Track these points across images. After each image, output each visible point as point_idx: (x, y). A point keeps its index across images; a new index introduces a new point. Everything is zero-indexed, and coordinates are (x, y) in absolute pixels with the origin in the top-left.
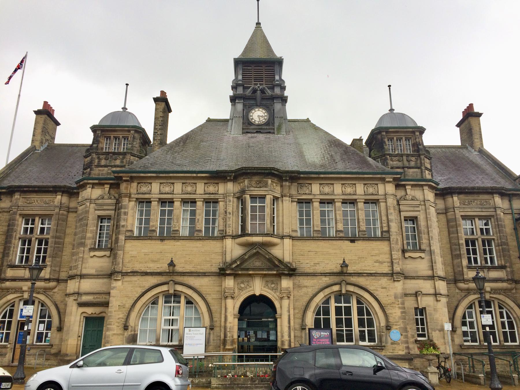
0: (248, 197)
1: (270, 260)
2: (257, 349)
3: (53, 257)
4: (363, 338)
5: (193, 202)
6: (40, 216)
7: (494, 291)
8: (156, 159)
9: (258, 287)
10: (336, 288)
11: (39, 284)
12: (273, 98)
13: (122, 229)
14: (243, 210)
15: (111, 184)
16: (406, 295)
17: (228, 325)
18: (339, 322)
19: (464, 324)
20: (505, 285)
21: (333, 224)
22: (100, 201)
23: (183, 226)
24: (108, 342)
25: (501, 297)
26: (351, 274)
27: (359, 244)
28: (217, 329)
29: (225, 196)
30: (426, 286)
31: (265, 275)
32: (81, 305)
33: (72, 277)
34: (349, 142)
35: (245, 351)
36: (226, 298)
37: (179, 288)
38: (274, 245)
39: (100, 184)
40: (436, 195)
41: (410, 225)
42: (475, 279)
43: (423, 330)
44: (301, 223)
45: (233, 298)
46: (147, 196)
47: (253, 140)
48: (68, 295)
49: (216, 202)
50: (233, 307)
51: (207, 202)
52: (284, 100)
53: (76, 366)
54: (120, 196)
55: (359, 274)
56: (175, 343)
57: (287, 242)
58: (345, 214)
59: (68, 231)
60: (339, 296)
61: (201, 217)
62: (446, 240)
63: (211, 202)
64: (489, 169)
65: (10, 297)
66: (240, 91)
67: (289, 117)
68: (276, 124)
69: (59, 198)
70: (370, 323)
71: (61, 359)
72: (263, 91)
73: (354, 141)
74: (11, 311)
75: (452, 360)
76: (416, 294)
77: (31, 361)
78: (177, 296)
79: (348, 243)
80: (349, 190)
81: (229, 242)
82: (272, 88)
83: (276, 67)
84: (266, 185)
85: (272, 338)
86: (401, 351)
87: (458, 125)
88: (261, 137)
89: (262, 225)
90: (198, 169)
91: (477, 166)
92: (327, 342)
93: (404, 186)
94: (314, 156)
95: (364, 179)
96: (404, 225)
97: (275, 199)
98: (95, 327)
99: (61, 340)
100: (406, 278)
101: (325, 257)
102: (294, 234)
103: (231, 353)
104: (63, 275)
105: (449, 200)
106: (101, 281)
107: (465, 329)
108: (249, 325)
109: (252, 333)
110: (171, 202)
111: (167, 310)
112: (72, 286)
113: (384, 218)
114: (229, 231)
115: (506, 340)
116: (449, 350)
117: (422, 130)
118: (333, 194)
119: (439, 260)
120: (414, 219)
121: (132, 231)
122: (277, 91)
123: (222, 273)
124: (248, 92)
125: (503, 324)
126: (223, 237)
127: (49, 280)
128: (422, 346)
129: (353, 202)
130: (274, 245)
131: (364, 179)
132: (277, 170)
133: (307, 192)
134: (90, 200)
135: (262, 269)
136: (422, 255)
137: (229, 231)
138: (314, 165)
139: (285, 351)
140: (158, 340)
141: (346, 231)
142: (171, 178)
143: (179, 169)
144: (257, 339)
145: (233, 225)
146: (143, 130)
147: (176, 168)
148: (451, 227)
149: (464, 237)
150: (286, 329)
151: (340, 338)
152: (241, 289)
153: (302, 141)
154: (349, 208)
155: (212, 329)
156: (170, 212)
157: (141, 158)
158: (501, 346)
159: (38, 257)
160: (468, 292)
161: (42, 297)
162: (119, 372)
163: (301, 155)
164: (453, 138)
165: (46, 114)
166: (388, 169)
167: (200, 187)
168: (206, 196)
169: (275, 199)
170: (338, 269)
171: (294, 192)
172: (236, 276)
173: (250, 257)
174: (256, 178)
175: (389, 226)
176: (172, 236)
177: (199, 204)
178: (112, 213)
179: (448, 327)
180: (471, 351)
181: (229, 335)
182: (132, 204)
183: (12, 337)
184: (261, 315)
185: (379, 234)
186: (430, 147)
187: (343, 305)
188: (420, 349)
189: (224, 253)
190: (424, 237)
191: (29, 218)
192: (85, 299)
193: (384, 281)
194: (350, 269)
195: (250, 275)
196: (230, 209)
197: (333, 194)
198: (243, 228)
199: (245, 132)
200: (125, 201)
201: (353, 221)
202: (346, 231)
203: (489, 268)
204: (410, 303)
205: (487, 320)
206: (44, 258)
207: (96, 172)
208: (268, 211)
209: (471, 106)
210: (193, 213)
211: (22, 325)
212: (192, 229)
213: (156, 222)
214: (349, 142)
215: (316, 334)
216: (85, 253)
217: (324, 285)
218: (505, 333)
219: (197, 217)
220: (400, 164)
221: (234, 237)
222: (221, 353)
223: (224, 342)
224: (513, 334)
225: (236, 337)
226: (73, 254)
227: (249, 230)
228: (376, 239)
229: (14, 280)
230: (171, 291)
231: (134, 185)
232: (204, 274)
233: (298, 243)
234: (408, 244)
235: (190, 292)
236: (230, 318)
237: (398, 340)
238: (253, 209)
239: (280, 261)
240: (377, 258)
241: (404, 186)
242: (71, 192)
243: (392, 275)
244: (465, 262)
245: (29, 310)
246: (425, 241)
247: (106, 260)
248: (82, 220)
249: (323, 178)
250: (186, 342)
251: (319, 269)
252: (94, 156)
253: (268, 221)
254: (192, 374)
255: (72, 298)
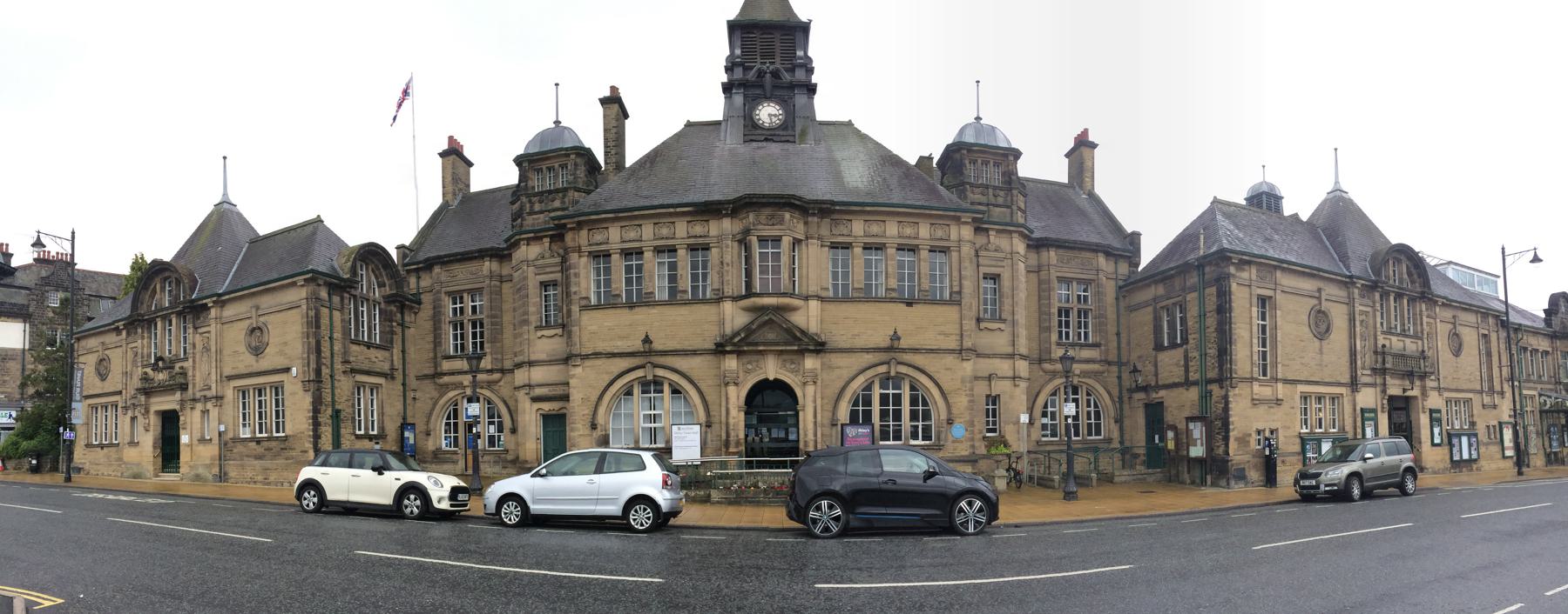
0: (754, 239)
1: (789, 331)
2: (772, 453)
3: (493, 341)
4: (915, 436)
5: (672, 250)
6: (469, 291)
7: (1084, 374)
8: (611, 193)
9: (771, 369)
10: (883, 369)
11: (481, 377)
12: (792, 86)
13: (574, 297)
14: (748, 259)
15: (552, 237)
16: (977, 378)
17: (731, 421)
18: (884, 415)
19: (1044, 415)
20: (1096, 367)
21: (882, 279)
22: (541, 262)
23: (658, 285)
24: (573, 446)
25: (1090, 381)
26: (904, 350)
27: (916, 308)
28: (715, 427)
29: (720, 238)
30: (1004, 367)
31: (781, 353)
32: (535, 399)
33: (519, 366)
34: (913, 161)
35: (755, 453)
36: (727, 384)
37: (660, 372)
38: (794, 309)
39: (538, 239)
40: (1028, 246)
41: (990, 285)
42: (1063, 359)
43: (994, 423)
44: (835, 277)
45: (736, 384)
46: (603, 247)
47: (761, 152)
48: (517, 388)
49: (706, 248)
50: (736, 396)
51: (693, 249)
52: (811, 89)
53: (537, 475)
54: (566, 250)
55: (916, 351)
56: (660, 445)
57: (814, 305)
58: (901, 265)
59: (506, 306)
60: (885, 380)
61: (685, 272)
62: (1035, 306)
63: (698, 248)
64: (1097, 219)
65: (452, 394)
66: (738, 73)
67: (820, 117)
68: (798, 129)
69: (488, 266)
70: (927, 415)
71: (520, 466)
72: (776, 74)
73: (921, 158)
74: (456, 411)
75: (1026, 459)
76: (990, 378)
77: (486, 469)
78: (657, 384)
79: (903, 306)
80: (908, 231)
81: (728, 306)
82: (792, 70)
83: (799, 36)
84: (781, 222)
85: (792, 437)
86: (963, 450)
87: (1067, 156)
88: (774, 148)
89: (777, 281)
90: (676, 201)
91: (1082, 213)
92: (867, 442)
93: (987, 230)
94: (856, 176)
95: (931, 216)
96: (983, 284)
97: (796, 242)
98: (555, 426)
99: (517, 444)
100: (979, 355)
101: (865, 326)
102: (824, 294)
103: (736, 458)
104: (508, 364)
105: (1044, 254)
106: (555, 368)
107: (1045, 421)
108: (761, 420)
109: (764, 430)
110: (640, 253)
111: (647, 404)
112: (521, 376)
113: (955, 274)
114: (728, 291)
115: (1090, 434)
116: (1023, 447)
117: (1017, 154)
118: (884, 236)
119: (1022, 333)
120: (995, 278)
121: (587, 298)
122: (800, 75)
123: (720, 350)
124: (751, 75)
125: (1089, 413)
126: (719, 299)
127: (491, 371)
128: (991, 443)
129: (913, 249)
130: (794, 309)
131: (931, 216)
132: (800, 199)
133: (845, 232)
134: (527, 262)
135: (777, 344)
136: (1002, 326)
137: (728, 291)
138: (856, 191)
139: (808, 454)
140: (637, 442)
141: (901, 289)
142: (636, 217)
143: (647, 203)
144: (772, 440)
145: (735, 284)
146: (589, 151)
147: (642, 203)
148: (1043, 291)
149: (1057, 305)
150: (810, 426)
151: (885, 436)
152: (747, 372)
153: (838, 155)
154: (907, 258)
155: (709, 425)
156: (640, 268)
157: (589, 192)
158: (1084, 442)
159: (475, 344)
160: (1054, 374)
161: (487, 393)
162: (591, 482)
163: (838, 176)
164: (1056, 171)
165: (454, 155)
166: (965, 205)
167: (682, 229)
168: (692, 241)
169: (796, 242)
170: (886, 343)
171: (825, 231)
172: (739, 353)
173: (760, 326)
174: (767, 211)
175: (961, 285)
176: (644, 301)
177: (681, 252)
178: (558, 276)
179: (1024, 418)
180: (1049, 448)
181: (732, 434)
182: (584, 260)
183: (461, 441)
184: (778, 407)
185: (947, 295)
186: (1028, 180)
187: (891, 391)
188: (988, 447)
189: (722, 323)
190: (1007, 302)
191: (456, 296)
192: (538, 392)
193: (950, 360)
194: (903, 344)
195: (760, 352)
196: (728, 259)
197: (884, 236)
198: (749, 285)
199: (748, 139)
200: (574, 257)
201: (911, 277)
202: (901, 289)
203: (1081, 346)
204: (982, 389)
205: (1070, 409)
206: (482, 343)
207: (530, 222)
208: (785, 259)
209: (1085, 132)
210: (673, 267)
211: (470, 427)
212: (673, 291)
213: (619, 284)
214: (913, 161)
215: (851, 431)
216: (530, 333)
217: (865, 365)
218: (1089, 425)
219: (680, 272)
220: (984, 199)
221: (735, 299)
222: (723, 458)
223: (727, 444)
224: (1098, 426)
225: (742, 436)
226: (515, 336)
227: (757, 288)
228: (942, 302)
229: (452, 374)
230: (650, 377)
231: (584, 233)
232: (694, 353)
233: (831, 307)
234: (986, 311)
235: (675, 377)
236: (734, 412)
237: (961, 437)
238: (763, 256)
239: (803, 332)
240: (942, 328)
241: (987, 230)
242: (501, 255)
243: (961, 352)
244: (1054, 337)
245: (474, 409)
246: (1007, 307)
247: (557, 339)
248: (521, 290)
249: (869, 213)
250: (675, 444)
251: (859, 343)
252: (524, 199)
253: (785, 274)
254: (684, 485)
255: (523, 392)
